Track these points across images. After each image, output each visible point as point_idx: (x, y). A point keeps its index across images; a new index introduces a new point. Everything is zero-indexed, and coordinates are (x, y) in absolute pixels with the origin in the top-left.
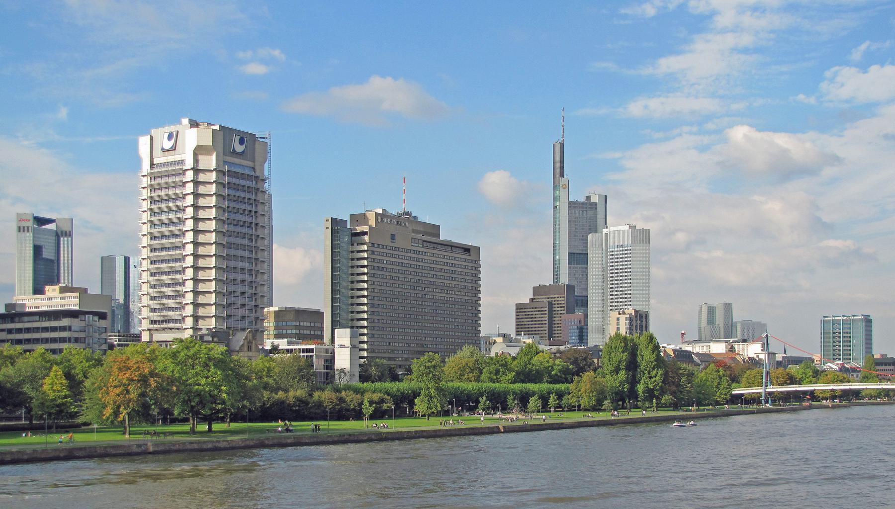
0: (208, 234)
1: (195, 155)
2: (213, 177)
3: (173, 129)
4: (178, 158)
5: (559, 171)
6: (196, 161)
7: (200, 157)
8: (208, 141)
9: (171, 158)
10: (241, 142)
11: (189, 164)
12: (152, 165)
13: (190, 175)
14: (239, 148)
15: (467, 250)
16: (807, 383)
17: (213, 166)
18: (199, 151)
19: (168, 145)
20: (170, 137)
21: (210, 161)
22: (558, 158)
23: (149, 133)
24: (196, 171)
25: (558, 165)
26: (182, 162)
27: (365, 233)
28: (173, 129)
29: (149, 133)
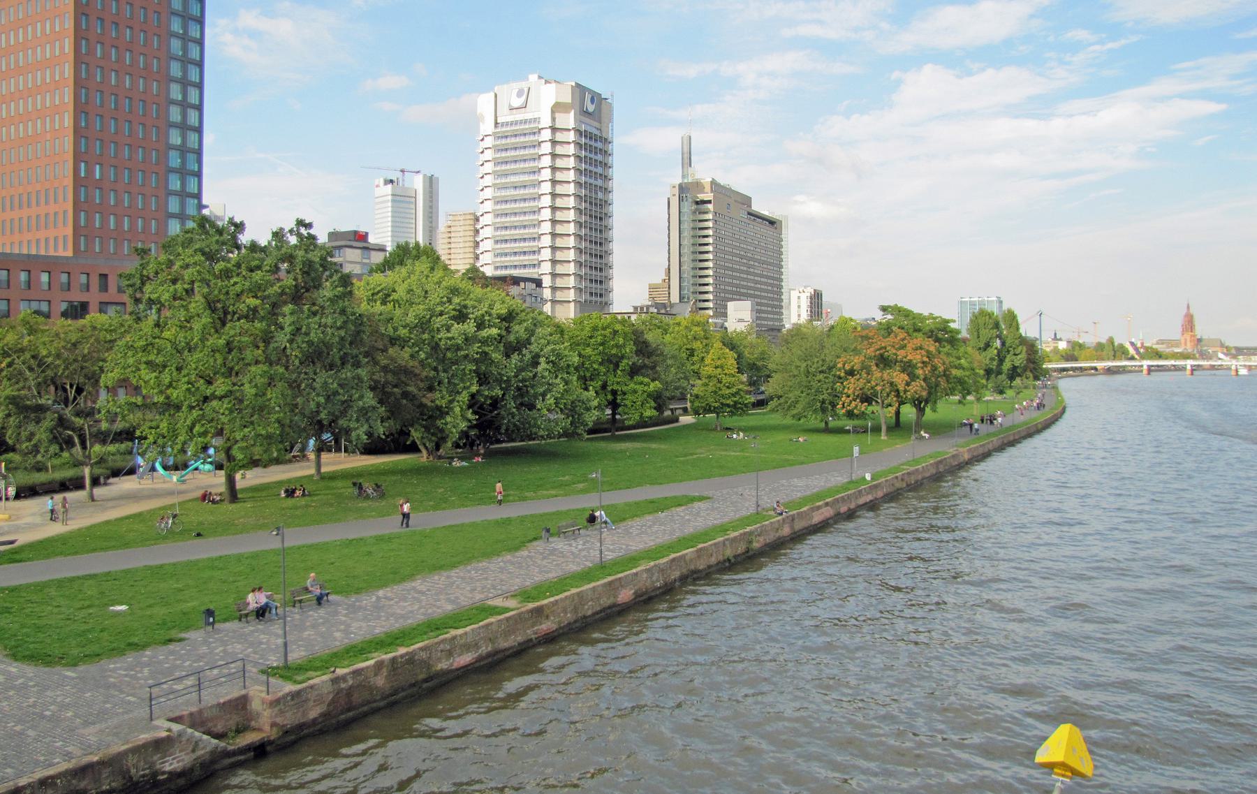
0: (566, 212)
1: (553, 112)
2: (571, 136)
3: (524, 85)
4: (528, 116)
5: (687, 161)
6: (554, 119)
7: (557, 115)
8: (567, 98)
9: (519, 116)
10: (592, 101)
11: (546, 121)
12: (496, 123)
13: (546, 135)
14: (591, 108)
15: (772, 222)
16: (137, 570)
17: (571, 125)
18: (557, 108)
19: (517, 102)
20: (520, 94)
21: (568, 120)
22: (686, 150)
23: (493, 90)
24: (554, 129)
25: (686, 156)
26: (536, 120)
27: (709, 202)
28: (524, 85)
29: (493, 90)
